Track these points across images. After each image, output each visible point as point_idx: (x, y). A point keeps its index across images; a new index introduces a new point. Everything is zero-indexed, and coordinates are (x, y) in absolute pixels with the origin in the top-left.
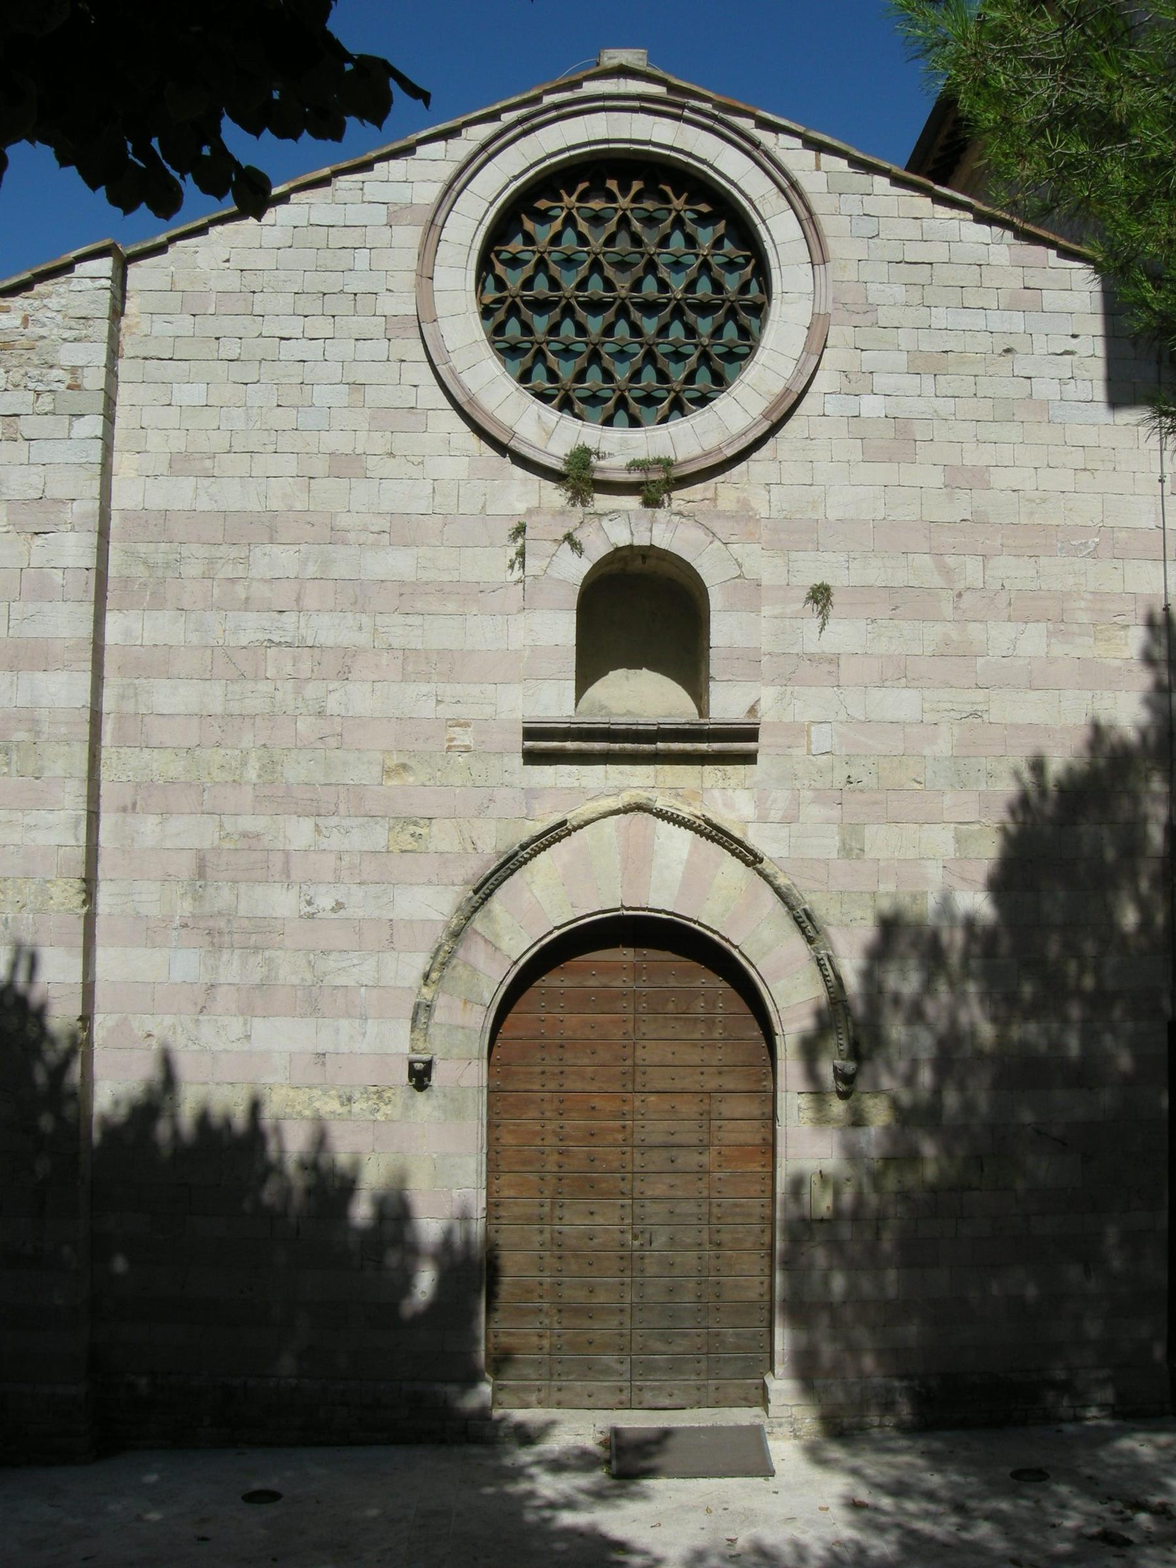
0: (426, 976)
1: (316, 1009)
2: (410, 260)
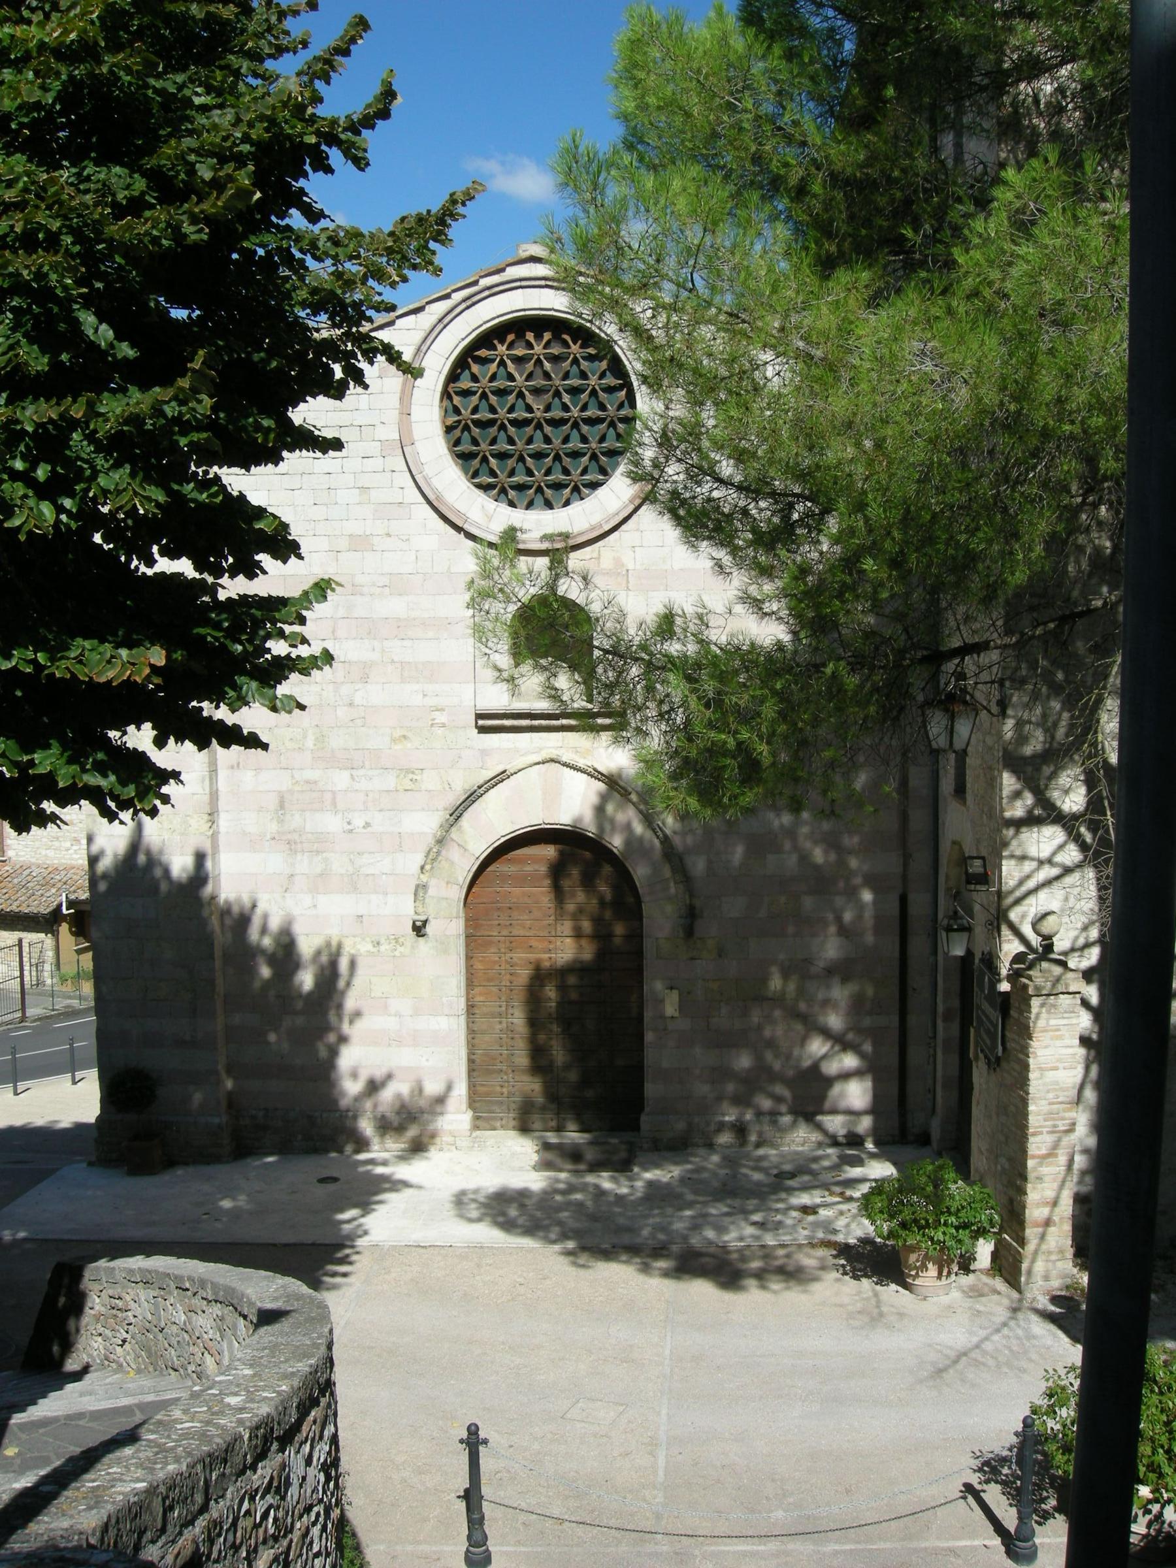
0: (422, 868)
1: (356, 889)
2: (394, 401)
